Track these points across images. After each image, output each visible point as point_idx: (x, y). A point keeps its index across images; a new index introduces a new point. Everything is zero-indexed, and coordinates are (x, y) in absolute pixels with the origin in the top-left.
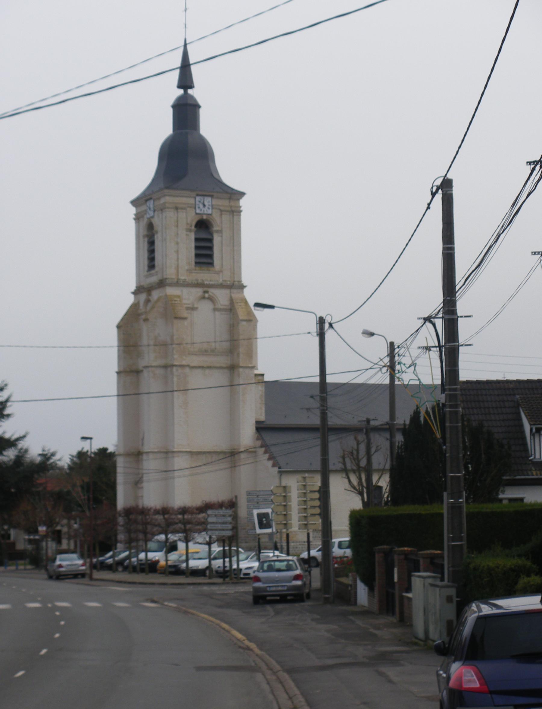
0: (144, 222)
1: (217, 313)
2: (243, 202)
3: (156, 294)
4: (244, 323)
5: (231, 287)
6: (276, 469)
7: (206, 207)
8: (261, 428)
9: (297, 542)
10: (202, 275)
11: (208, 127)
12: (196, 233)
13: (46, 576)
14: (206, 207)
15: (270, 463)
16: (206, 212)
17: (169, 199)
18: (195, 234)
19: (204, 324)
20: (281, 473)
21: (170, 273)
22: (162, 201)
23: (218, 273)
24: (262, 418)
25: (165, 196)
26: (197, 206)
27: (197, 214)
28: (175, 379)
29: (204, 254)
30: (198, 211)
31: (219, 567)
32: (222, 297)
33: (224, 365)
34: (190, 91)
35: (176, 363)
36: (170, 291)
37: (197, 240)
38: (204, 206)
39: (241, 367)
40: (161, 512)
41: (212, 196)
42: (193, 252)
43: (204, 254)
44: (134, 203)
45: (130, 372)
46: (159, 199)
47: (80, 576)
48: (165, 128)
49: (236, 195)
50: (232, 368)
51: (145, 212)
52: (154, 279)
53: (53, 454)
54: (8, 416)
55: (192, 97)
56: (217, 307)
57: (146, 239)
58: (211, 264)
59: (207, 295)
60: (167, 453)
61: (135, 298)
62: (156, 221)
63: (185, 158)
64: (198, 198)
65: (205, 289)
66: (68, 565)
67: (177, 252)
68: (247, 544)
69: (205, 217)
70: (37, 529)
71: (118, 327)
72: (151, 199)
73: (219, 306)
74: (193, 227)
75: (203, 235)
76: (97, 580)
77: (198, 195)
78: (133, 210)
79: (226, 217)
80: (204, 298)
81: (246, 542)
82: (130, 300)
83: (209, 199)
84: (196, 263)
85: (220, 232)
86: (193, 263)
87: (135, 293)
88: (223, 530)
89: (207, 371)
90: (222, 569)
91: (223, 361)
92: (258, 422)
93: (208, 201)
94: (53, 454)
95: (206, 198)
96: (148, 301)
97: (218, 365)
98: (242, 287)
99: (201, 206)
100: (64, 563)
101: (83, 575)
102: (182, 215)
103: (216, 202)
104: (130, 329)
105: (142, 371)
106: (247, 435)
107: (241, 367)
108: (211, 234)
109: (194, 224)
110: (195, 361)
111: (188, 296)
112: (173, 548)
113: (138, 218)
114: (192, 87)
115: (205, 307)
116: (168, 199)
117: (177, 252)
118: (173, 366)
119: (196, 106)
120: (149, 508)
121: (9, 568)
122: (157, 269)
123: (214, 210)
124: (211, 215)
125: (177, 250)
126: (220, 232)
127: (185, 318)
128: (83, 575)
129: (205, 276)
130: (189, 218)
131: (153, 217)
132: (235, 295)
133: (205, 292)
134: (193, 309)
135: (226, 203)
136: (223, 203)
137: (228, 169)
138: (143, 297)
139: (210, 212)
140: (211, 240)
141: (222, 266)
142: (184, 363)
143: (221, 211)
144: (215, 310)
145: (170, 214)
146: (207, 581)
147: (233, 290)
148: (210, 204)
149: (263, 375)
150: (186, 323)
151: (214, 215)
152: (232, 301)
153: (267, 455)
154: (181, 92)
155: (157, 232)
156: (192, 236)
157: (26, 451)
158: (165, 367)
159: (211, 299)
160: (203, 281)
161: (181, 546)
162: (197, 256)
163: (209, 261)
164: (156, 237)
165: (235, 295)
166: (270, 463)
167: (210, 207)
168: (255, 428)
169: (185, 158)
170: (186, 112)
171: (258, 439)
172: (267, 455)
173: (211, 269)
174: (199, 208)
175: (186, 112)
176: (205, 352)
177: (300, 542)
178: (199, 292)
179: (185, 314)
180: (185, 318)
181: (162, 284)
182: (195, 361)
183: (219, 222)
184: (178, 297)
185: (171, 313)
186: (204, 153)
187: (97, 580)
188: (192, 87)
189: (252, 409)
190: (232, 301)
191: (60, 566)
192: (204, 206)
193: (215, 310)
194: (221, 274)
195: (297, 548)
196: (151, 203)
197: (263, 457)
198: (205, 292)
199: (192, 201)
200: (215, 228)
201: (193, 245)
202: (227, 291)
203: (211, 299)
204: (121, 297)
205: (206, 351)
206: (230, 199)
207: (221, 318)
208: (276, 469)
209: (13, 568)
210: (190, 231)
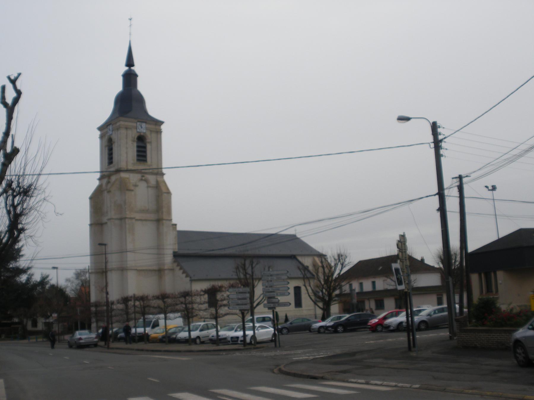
0: (106, 138)
1: (150, 189)
2: (163, 127)
3: (113, 178)
4: (165, 194)
6: (188, 279)
7: (143, 128)
8: (176, 255)
11: (142, 86)
12: (137, 142)
13: (67, 346)
14: (143, 128)
15: (184, 275)
17: (123, 123)
19: (142, 196)
20: (191, 281)
21: (123, 165)
22: (118, 124)
24: (176, 250)
25: (120, 121)
27: (138, 132)
28: (127, 226)
29: (142, 155)
30: (138, 130)
31: (213, 336)
32: (152, 179)
34: (132, 68)
35: (127, 216)
36: (123, 175)
38: (142, 128)
39: (165, 220)
40: (160, 297)
41: (146, 123)
42: (135, 154)
43: (142, 155)
44: (100, 129)
45: (98, 224)
46: (116, 123)
47: (93, 346)
48: (118, 87)
49: (159, 123)
50: (159, 221)
51: (107, 132)
52: (113, 169)
53: (47, 277)
54: (22, 256)
55: (134, 71)
57: (107, 148)
58: (145, 161)
59: (143, 178)
60: (123, 269)
61: (100, 182)
62: (114, 137)
63: (129, 101)
64: (138, 123)
66: (86, 338)
67: (127, 153)
69: (142, 134)
71: (91, 198)
72: (110, 124)
74: (135, 139)
75: (141, 144)
76: (113, 348)
77: (139, 121)
78: (98, 133)
79: (154, 135)
80: (142, 180)
82: (97, 183)
87: (100, 179)
88: (242, 304)
90: (215, 338)
91: (153, 216)
93: (144, 125)
94: (47, 277)
96: (108, 182)
99: (140, 128)
100: (83, 337)
101: (95, 345)
102: (129, 132)
103: (148, 126)
104: (97, 200)
105: (106, 223)
106: (168, 259)
107: (165, 220)
108: (146, 144)
109: (136, 137)
110: (138, 216)
111: (133, 178)
112: (156, 325)
113: (102, 137)
114: (133, 65)
115: (143, 185)
116: (122, 123)
117: (127, 153)
118: (125, 218)
119: (136, 76)
120: (146, 295)
121: (31, 341)
122: (114, 163)
125: (126, 153)
126: (150, 143)
127: (132, 190)
128: (95, 345)
129: (141, 167)
130: (133, 134)
131: (112, 134)
132: (159, 178)
133: (143, 176)
134: (136, 186)
136: (152, 127)
137: (153, 109)
138: (105, 181)
139: (145, 131)
141: (151, 162)
142: (132, 216)
143: (151, 131)
144: (148, 187)
145: (123, 131)
146: (253, 347)
149: (176, 225)
150: (133, 193)
152: (157, 182)
153: (182, 271)
154: (127, 68)
155: (114, 142)
157: (33, 275)
158: (121, 219)
159: (146, 181)
161: (162, 322)
162: (138, 156)
164: (113, 146)
165: (159, 178)
166: (184, 275)
169: (129, 101)
170: (130, 78)
171: (175, 262)
172: (182, 271)
175: (130, 78)
176: (142, 211)
178: (139, 176)
179: (132, 188)
180: (132, 190)
181: (118, 171)
182: (138, 216)
183: (150, 137)
184: (128, 178)
185: (124, 187)
186: (140, 100)
187: (113, 348)
188: (133, 65)
189: (170, 245)
190: (157, 182)
191: (80, 339)
192: (142, 128)
196: (111, 127)
197: (179, 273)
198: (143, 176)
199: (135, 124)
200: (148, 141)
201: (135, 149)
203: (146, 181)
204: (92, 183)
207: (152, 192)
208: (188, 279)
209: (34, 340)
210: (134, 141)
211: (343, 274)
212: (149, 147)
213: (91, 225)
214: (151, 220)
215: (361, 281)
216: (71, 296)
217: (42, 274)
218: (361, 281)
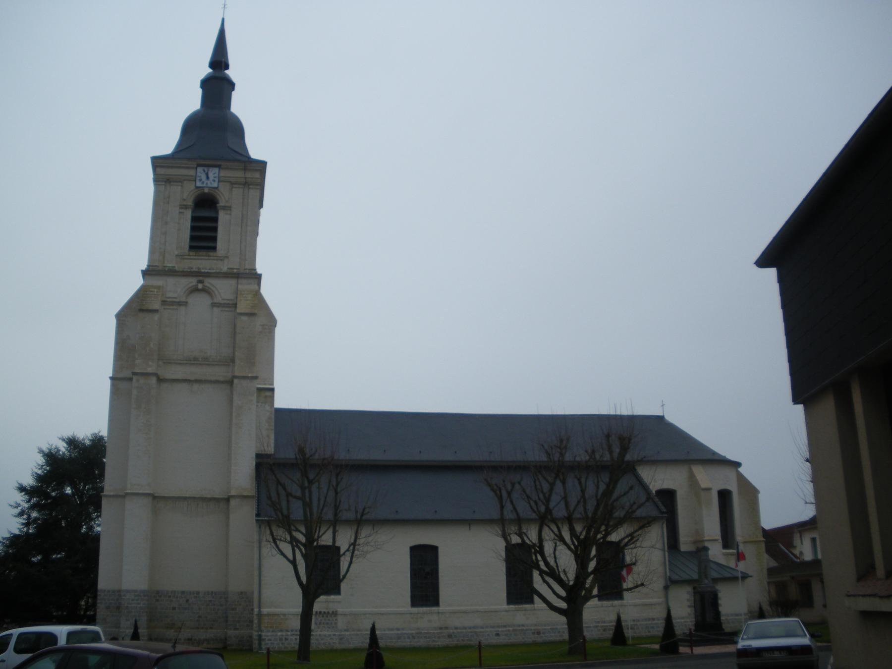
1: (215, 309)
4: (245, 318)
5: (235, 275)
9: (287, 631)
10: (199, 261)
16: (209, 185)
18: (193, 212)
23: (222, 259)
24: (271, 450)
26: (198, 179)
27: (197, 188)
30: (199, 184)
32: (224, 289)
33: (222, 379)
37: (194, 219)
38: (208, 178)
41: (219, 166)
48: (193, 102)
49: (261, 166)
56: (215, 301)
58: (214, 248)
64: (200, 169)
65: (201, 278)
68: (237, 632)
69: (206, 191)
70: (678, 649)
73: (218, 299)
77: (199, 165)
79: (237, 192)
81: (236, 629)
83: (216, 170)
84: (192, 248)
85: (227, 208)
86: (187, 247)
89: (196, 387)
92: (258, 456)
93: (213, 173)
95: (211, 169)
97: (213, 378)
98: (258, 278)
99: (204, 177)
108: (217, 212)
123: (221, 184)
124: (217, 188)
129: (202, 263)
135: (240, 174)
139: (215, 185)
140: (215, 220)
143: (232, 183)
144: (214, 305)
147: (240, 281)
148: (217, 175)
151: (221, 189)
156: (188, 214)
160: (199, 268)
162: (193, 238)
163: (211, 244)
167: (217, 180)
168: (254, 463)
170: (217, 86)
173: (211, 254)
174: (200, 180)
175: (217, 86)
176: (194, 361)
177: (292, 631)
184: (158, 287)
186: (236, 129)
189: (250, 441)
192: (208, 178)
193: (214, 305)
194: (226, 261)
195: (286, 639)
199: (192, 172)
200: (222, 203)
202: (233, 282)
205: (196, 359)
206: (245, 169)
211: (531, 576)
212: (222, 217)
213: (112, 378)
214: (216, 382)
215: (427, 620)
216: (585, 633)
217: (41, 451)
218: (427, 620)
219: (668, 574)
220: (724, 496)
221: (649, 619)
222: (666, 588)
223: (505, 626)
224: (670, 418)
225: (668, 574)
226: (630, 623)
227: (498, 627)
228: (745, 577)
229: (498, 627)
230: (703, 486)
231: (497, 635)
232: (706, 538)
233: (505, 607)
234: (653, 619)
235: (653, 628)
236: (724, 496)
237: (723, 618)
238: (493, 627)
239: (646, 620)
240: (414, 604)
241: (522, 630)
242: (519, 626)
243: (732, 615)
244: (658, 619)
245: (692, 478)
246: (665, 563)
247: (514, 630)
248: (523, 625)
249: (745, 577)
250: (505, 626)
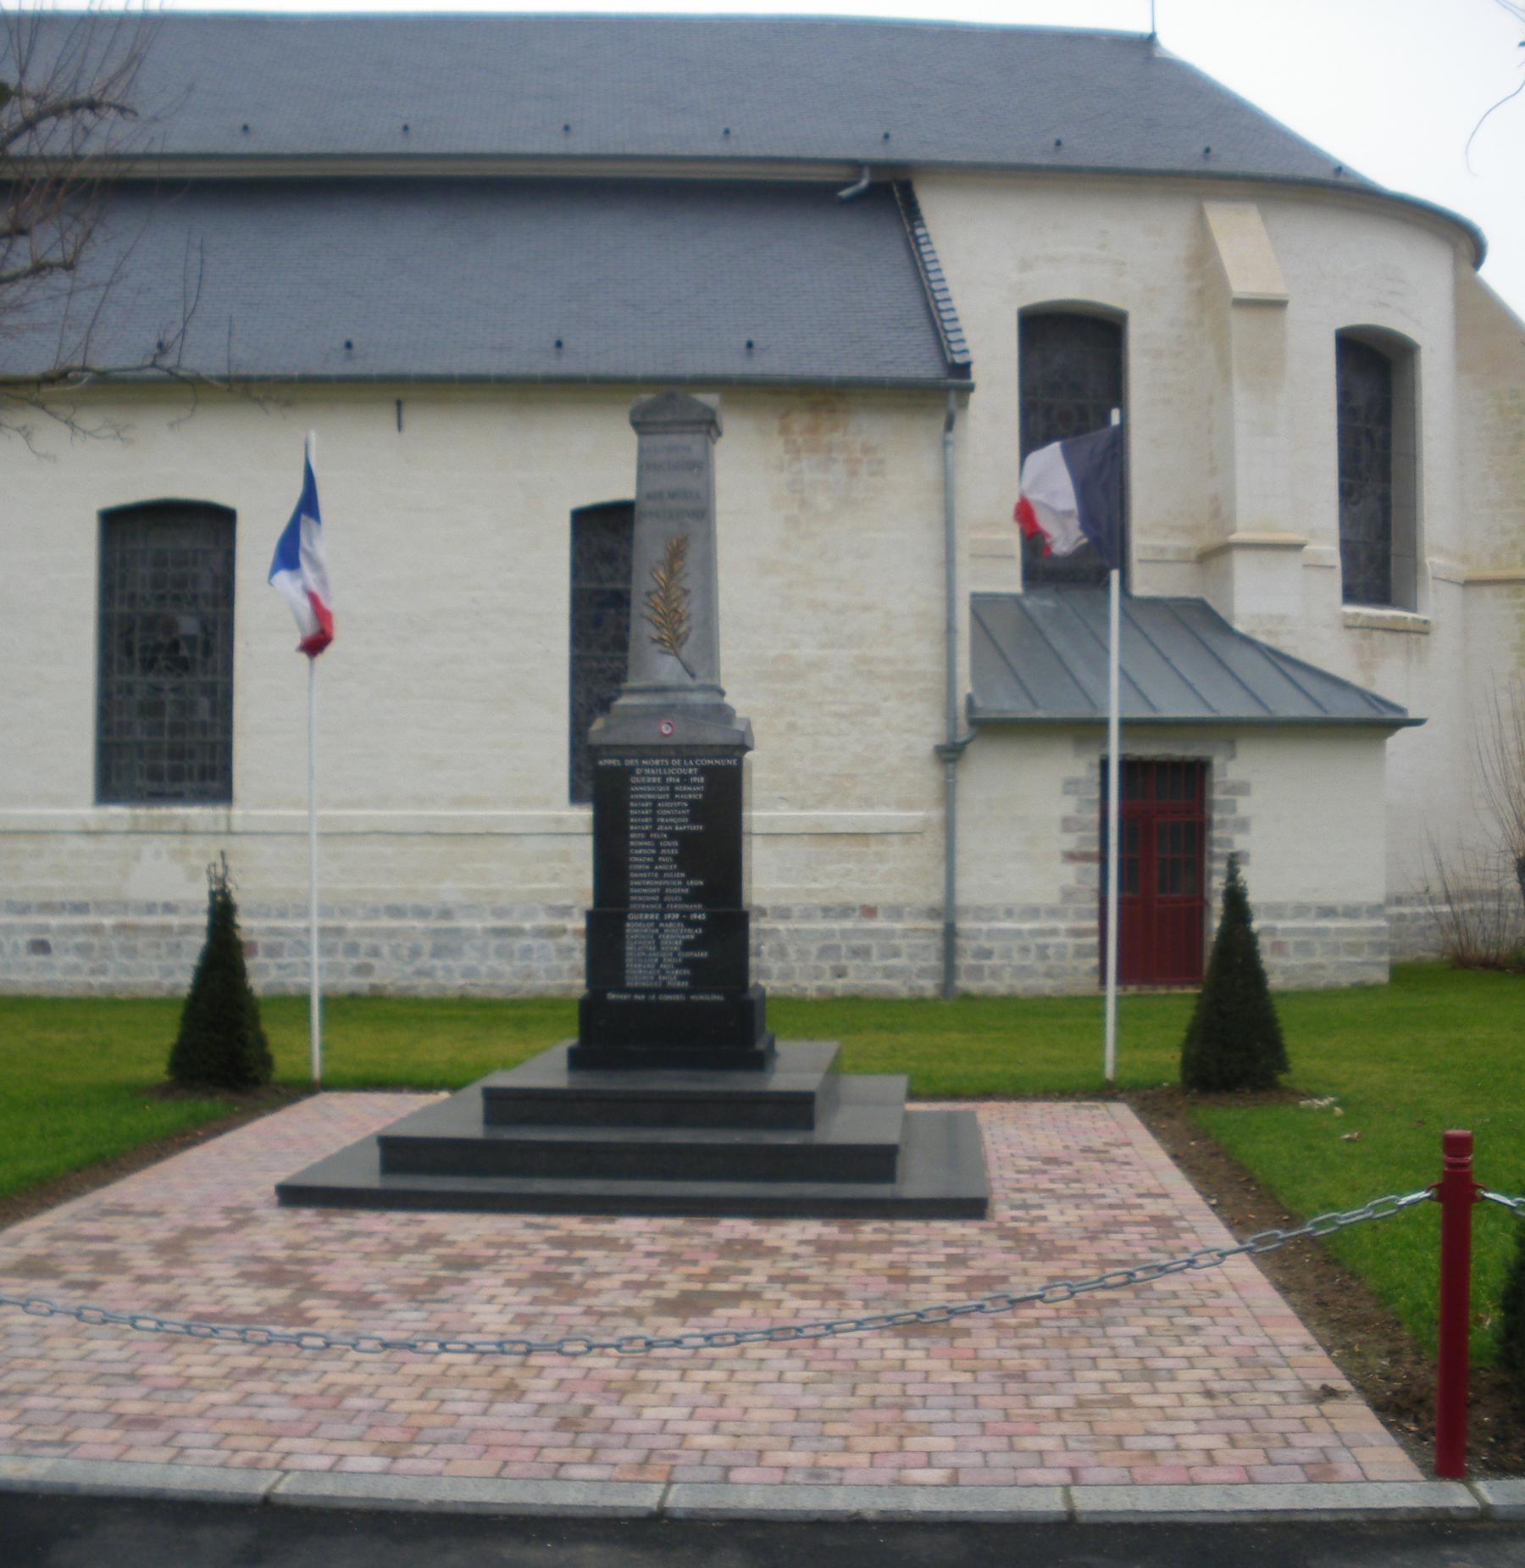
219: (965, 687)
220: (1373, 369)
221: (845, 911)
222: (950, 754)
223: (80, 908)
224: (1176, 44)
225: (965, 687)
226: (316, 976)
227: (47, 908)
228: (1377, 724)
229: (47, 908)
230: (1242, 285)
231: (41, 947)
232: (1238, 536)
233: (87, 811)
234: (869, 912)
235: (861, 953)
236: (1373, 369)
237: (1255, 925)
238: (24, 909)
239: (827, 911)
240: (109, 788)
241: (166, 929)
242: (150, 908)
243: (1301, 910)
244: (896, 912)
245: (1203, 260)
246: (950, 629)
247: (121, 928)
248: (169, 908)
249: (1377, 724)
250: (80, 908)
